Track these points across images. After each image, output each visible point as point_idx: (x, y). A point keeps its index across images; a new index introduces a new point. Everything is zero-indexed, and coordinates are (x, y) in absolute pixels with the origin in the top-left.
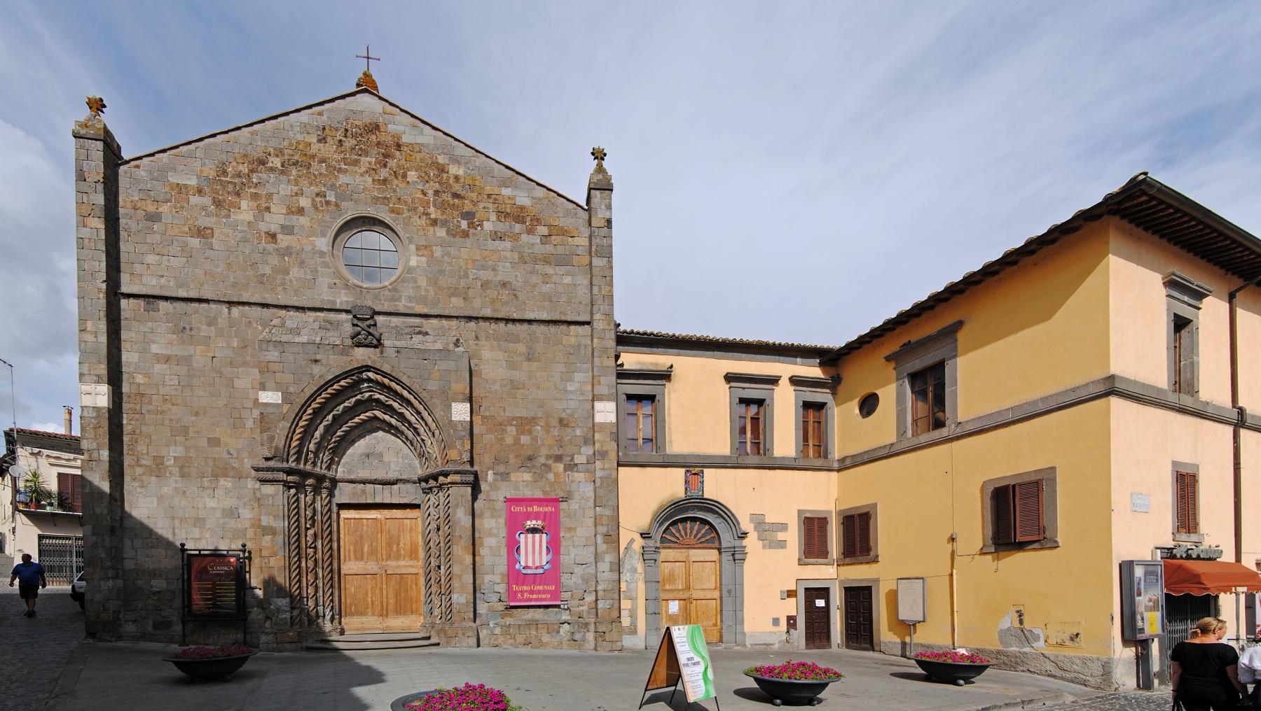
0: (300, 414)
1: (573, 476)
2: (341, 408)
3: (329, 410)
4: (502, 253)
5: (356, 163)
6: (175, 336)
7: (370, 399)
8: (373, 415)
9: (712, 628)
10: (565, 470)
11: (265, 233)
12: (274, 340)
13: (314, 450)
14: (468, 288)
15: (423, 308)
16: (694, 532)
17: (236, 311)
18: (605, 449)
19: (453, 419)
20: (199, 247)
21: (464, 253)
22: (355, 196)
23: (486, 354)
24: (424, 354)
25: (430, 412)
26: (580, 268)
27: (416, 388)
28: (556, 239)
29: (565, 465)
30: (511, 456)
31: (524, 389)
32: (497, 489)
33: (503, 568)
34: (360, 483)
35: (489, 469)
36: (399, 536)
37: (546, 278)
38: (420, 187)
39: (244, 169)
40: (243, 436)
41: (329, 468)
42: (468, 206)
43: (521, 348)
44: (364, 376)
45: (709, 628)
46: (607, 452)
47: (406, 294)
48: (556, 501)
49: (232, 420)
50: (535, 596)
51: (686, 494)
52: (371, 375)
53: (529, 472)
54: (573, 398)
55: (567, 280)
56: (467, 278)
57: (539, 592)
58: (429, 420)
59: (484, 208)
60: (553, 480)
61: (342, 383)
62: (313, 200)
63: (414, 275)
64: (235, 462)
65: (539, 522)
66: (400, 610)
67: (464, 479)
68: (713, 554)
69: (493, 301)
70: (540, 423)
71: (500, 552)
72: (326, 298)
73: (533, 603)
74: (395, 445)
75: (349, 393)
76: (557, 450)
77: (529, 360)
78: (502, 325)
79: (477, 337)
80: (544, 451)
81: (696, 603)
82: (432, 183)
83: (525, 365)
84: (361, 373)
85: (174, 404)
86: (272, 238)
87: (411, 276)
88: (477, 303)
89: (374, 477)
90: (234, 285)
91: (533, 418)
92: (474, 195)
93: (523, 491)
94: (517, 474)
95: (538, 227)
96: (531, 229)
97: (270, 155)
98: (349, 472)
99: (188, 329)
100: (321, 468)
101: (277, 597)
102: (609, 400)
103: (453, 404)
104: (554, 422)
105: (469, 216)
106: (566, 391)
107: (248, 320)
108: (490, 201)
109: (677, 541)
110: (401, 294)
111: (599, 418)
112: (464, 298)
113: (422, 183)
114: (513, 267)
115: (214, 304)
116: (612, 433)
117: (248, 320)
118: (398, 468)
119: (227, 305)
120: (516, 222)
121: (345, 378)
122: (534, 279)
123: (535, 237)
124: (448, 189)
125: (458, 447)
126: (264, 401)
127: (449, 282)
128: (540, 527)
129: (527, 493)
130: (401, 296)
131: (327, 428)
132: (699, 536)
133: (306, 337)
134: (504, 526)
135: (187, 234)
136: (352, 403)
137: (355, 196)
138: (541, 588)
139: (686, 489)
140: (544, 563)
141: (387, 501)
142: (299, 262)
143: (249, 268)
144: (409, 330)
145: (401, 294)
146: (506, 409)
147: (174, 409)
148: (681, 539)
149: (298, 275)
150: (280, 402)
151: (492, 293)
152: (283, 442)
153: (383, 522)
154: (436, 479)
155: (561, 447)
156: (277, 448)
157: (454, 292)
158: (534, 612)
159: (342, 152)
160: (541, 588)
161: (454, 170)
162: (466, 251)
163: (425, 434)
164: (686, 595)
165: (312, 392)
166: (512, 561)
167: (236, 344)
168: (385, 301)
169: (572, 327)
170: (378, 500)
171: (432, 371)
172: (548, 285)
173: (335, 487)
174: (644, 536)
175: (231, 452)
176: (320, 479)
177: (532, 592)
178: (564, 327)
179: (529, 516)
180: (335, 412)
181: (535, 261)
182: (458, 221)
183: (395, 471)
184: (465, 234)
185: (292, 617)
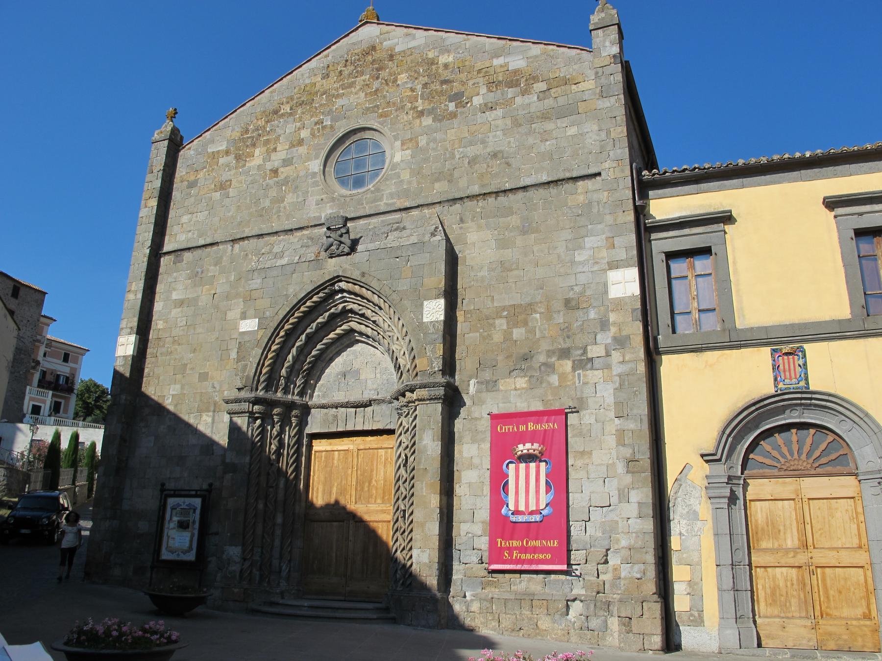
1: (585, 376)
2: (314, 325)
5: (351, 85)
6: (190, 281)
9: (862, 623)
10: (574, 369)
11: (270, 170)
12: (259, 268)
13: (285, 375)
15: (405, 202)
16: (806, 448)
18: (624, 333)
19: (425, 320)
21: (451, 134)
22: (348, 113)
23: (472, 237)
24: (395, 252)
26: (588, 114)
28: (557, 91)
29: (574, 361)
30: (500, 358)
32: (482, 402)
33: (484, 514)
34: (332, 408)
35: (471, 378)
36: (372, 471)
37: (545, 136)
38: (409, 86)
39: (261, 123)
40: (227, 368)
41: (302, 394)
42: (457, 87)
43: (514, 220)
45: (854, 622)
46: (628, 337)
47: (387, 192)
48: (563, 414)
49: (220, 352)
50: (529, 556)
51: (776, 386)
53: (525, 376)
54: (584, 270)
55: (572, 131)
57: (534, 550)
59: (474, 84)
60: (557, 384)
61: (315, 299)
62: (312, 129)
65: (536, 445)
67: (432, 393)
68: (846, 485)
69: (482, 176)
70: (539, 310)
73: (526, 567)
76: (562, 342)
78: (491, 200)
80: (545, 346)
81: (823, 574)
82: (421, 78)
83: (519, 241)
84: (333, 284)
85: (179, 344)
86: (275, 173)
87: (394, 172)
88: (463, 183)
91: (530, 304)
92: (463, 76)
93: (516, 403)
94: (508, 380)
95: (534, 85)
96: (526, 89)
97: (282, 104)
99: (200, 272)
100: (293, 394)
102: (630, 266)
103: (425, 303)
104: (558, 305)
105: (457, 98)
106: (573, 262)
107: (246, 253)
108: (481, 75)
109: (776, 464)
110: (383, 193)
111: (615, 292)
113: (411, 82)
114: (504, 134)
115: (222, 245)
116: (634, 310)
117: (246, 253)
118: (375, 386)
120: (509, 88)
121: (318, 293)
122: (531, 140)
123: (531, 96)
124: (437, 78)
125: (428, 354)
126: (243, 330)
127: (433, 167)
128: (536, 452)
129: (522, 406)
130: (383, 195)
131: (301, 350)
132: (817, 453)
137: (348, 113)
138: (537, 543)
139: (776, 379)
140: (542, 506)
141: (359, 427)
144: (386, 229)
145: (383, 193)
147: (179, 348)
148: (782, 460)
150: (256, 329)
151: (481, 167)
152: (254, 371)
155: (568, 337)
156: (248, 377)
157: (438, 177)
158: (529, 580)
159: (341, 80)
160: (537, 543)
161: (443, 59)
162: (454, 131)
164: (802, 559)
165: (285, 313)
166: (497, 503)
168: (367, 204)
169: (580, 183)
170: (350, 427)
171: (403, 269)
172: (548, 143)
173: (308, 413)
174: (708, 458)
175: (215, 386)
176: (291, 406)
177: (523, 550)
178: (569, 186)
179: (523, 438)
180: (308, 331)
181: (531, 121)
182: (445, 105)
183: (370, 390)
184: (453, 115)
185: (242, 570)
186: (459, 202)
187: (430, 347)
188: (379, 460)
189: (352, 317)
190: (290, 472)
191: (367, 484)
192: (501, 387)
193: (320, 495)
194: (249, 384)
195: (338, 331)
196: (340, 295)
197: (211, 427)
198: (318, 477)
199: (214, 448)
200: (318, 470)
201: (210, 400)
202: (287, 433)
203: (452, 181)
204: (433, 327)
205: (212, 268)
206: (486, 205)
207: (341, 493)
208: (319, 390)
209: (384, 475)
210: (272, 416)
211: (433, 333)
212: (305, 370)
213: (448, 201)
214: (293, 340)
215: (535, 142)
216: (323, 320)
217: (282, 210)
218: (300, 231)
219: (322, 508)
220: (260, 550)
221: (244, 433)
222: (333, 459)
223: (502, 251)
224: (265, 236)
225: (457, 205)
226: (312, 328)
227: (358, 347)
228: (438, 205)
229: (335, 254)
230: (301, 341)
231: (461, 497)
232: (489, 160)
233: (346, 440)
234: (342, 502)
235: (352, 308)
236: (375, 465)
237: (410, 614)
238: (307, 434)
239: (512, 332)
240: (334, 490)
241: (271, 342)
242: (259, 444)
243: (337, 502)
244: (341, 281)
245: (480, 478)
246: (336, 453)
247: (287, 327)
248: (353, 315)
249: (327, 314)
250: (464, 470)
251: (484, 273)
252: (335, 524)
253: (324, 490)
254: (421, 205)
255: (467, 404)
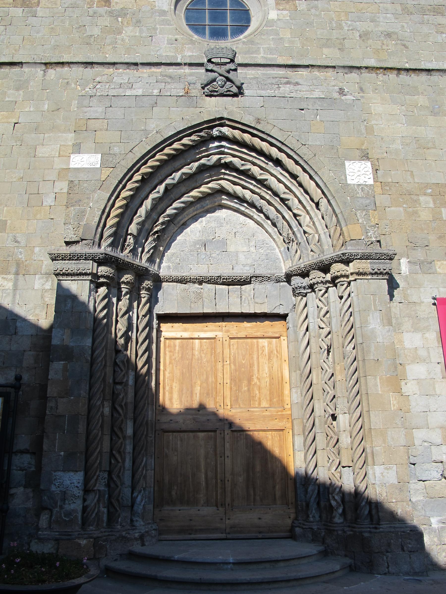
0: (125, 181)
2: (177, 176)
3: (161, 178)
4: (381, 5)
7: (219, 165)
8: (218, 187)
12: (98, 94)
13: (135, 234)
14: (344, 39)
17: (52, 72)
19: (349, 182)
20: (21, 15)
25: (312, 173)
27: (291, 142)
31: (435, 148)
34: (194, 283)
36: (252, 365)
40: (38, 216)
41: (151, 260)
43: (422, 100)
44: (215, 132)
52: (225, 130)
56: (341, 28)
58: (311, 186)
61: (186, 141)
63: (275, 28)
64: (21, 253)
66: (255, 495)
67: (376, 266)
69: (377, 51)
71: (434, 388)
72: (164, 54)
74: (245, 229)
75: (189, 156)
77: (434, 113)
78: (392, 76)
79: (361, 89)
83: (431, 120)
84: (212, 128)
89: (214, 272)
90: (55, 47)
98: (176, 268)
101: (64, 471)
103: (347, 163)
107: (66, 81)
110: (259, 46)
112: (339, 49)
115: (28, 67)
117: (66, 81)
118: (249, 262)
119: (43, 67)
121: (190, 135)
122: (425, 29)
125: (360, 221)
126: (76, 166)
131: (157, 202)
133: (141, 90)
134: (436, 344)
135: (10, 4)
136: (194, 169)
142: (134, 20)
143: (74, 31)
146: (414, 173)
149: (132, 34)
150: (98, 166)
152: (97, 219)
153: (226, 343)
154: (325, 269)
156: (86, 226)
163: (300, 207)
167: (46, 107)
170: (222, 309)
175: (19, 239)
180: (168, 181)
183: (244, 265)
186: (355, 71)
187: (362, 212)
188: (260, 352)
189: (225, 174)
190: (140, 365)
191: (245, 383)
192: (438, 270)
193: (175, 396)
194: (90, 236)
195: (204, 189)
196: (216, 144)
197: (11, 295)
198: (172, 372)
199: (18, 324)
200: (170, 363)
201: (10, 258)
202: (135, 310)
203: (343, 50)
204: (362, 191)
205: (12, 91)
206: (387, 80)
207: (208, 394)
208: (169, 260)
209: (269, 370)
210: (119, 284)
211: (362, 198)
212: (157, 232)
213: (344, 67)
214: (148, 189)
215: (430, 32)
216: (190, 171)
217: (119, 42)
218: (149, 67)
219: (180, 414)
220: (106, 475)
221: (83, 303)
222: (193, 349)
223: (414, 127)
224: (96, 66)
225: (353, 74)
226: (173, 179)
227: (222, 213)
228: (331, 70)
229: (217, 92)
230: (158, 192)
231: (410, 397)
232: (383, 39)
233: (211, 325)
234: (211, 405)
235: (231, 162)
236: (255, 358)
237: (385, 558)
238: (157, 314)
239: (441, 211)
240: (197, 389)
241: (121, 186)
242: (105, 320)
243: (202, 407)
244: (222, 125)
245: (429, 373)
246: (197, 341)
247: (144, 170)
248: (227, 172)
249: (196, 164)
250: (409, 364)
251: (397, 145)
252: (201, 435)
253: (181, 391)
254: (312, 66)
255: (401, 286)
